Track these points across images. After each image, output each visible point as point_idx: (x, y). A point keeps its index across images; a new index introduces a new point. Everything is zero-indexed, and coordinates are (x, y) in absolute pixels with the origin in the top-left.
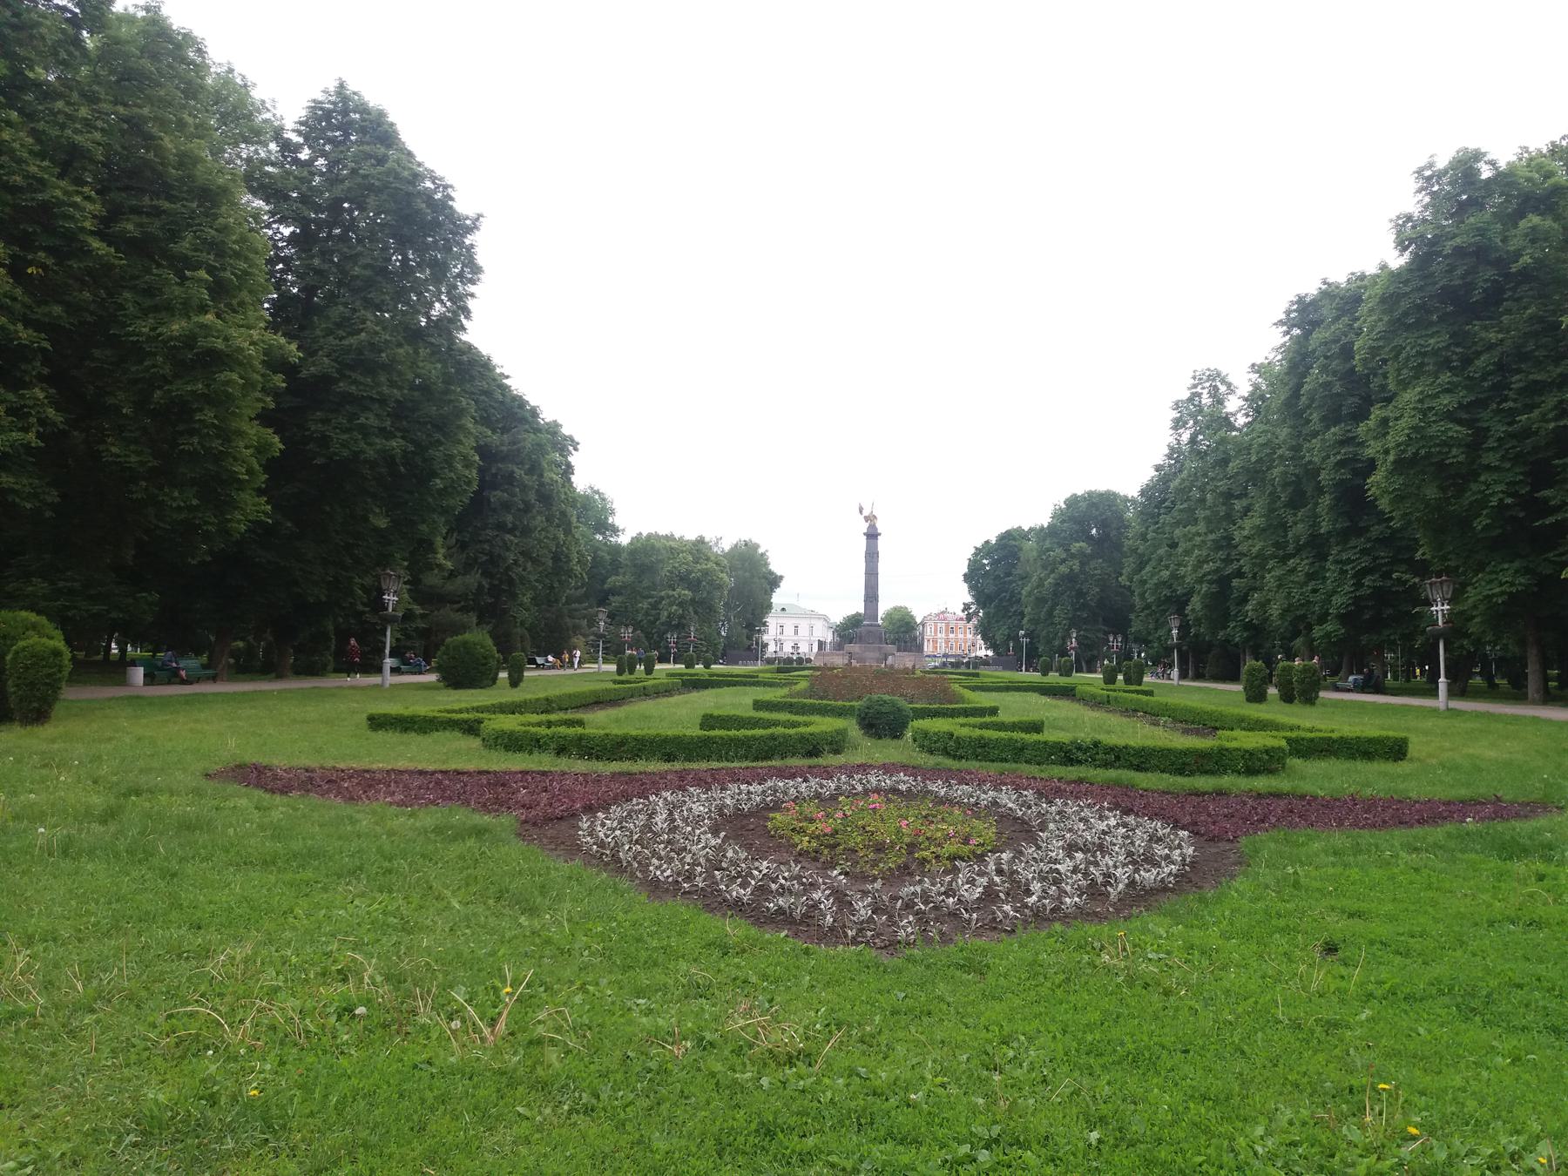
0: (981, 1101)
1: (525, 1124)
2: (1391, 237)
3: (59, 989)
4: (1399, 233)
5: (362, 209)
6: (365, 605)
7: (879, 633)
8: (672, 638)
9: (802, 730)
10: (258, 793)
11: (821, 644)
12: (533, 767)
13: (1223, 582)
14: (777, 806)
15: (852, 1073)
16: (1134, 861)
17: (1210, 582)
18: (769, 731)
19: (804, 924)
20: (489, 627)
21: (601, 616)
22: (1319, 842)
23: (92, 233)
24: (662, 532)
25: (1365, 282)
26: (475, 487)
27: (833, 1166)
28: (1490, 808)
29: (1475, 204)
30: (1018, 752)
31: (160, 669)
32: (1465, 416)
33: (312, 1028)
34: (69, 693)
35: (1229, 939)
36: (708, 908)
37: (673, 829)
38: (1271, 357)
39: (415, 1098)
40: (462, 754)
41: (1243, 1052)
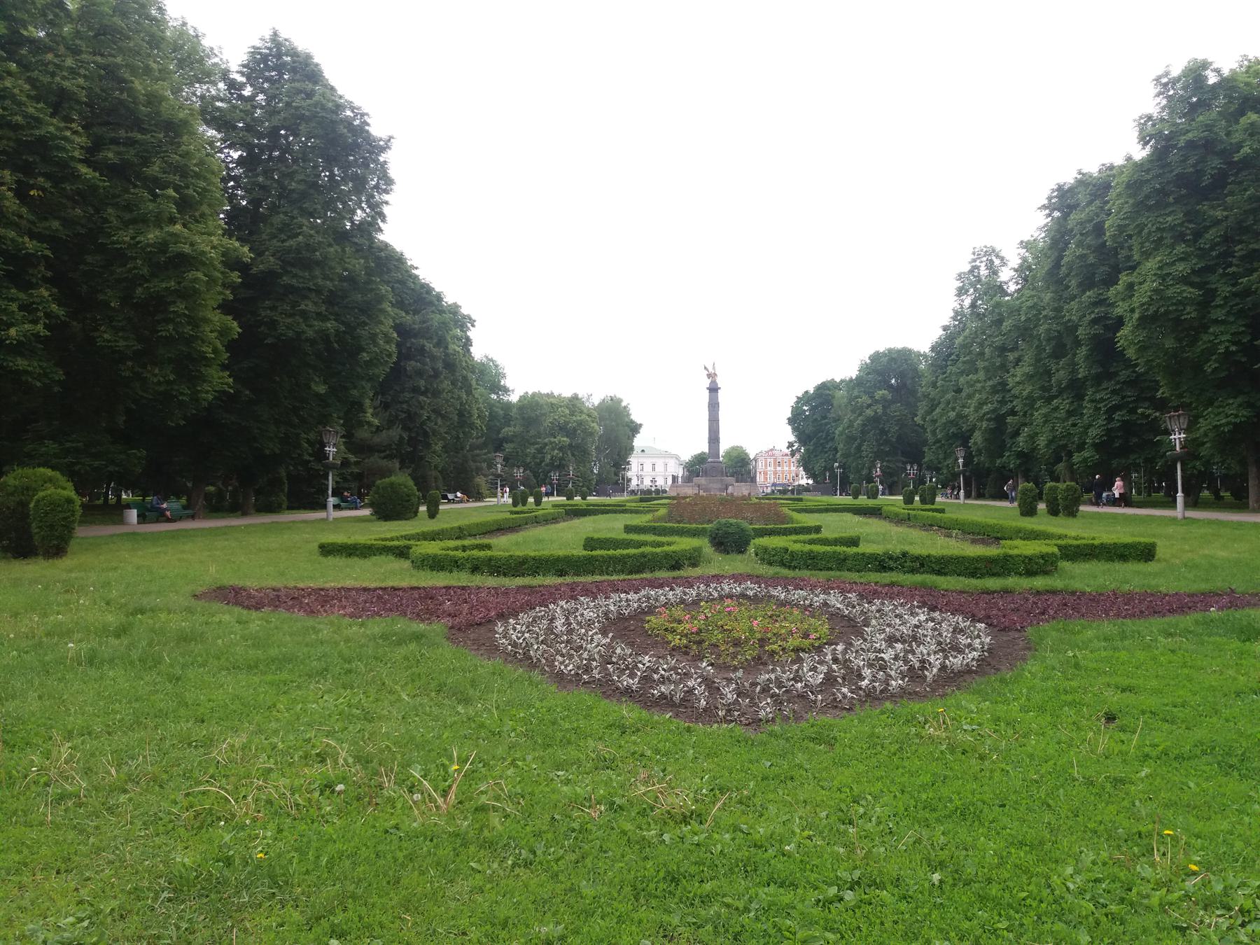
0: (842, 850)
1: (478, 876)
2: (1135, 134)
3: (96, 773)
4: (1141, 131)
5: (296, 135)
6: (310, 455)
8: (555, 476)
9: (666, 548)
10: (237, 610)
11: (674, 478)
12: (454, 583)
13: (1000, 420)
14: (651, 611)
15: (736, 829)
16: (943, 649)
18: (641, 550)
19: (683, 706)
20: (410, 471)
21: (498, 460)
22: (1093, 631)
23: (80, 161)
24: (544, 391)
25: (1114, 171)
26: (395, 359)
27: (728, 906)
28: (1226, 599)
29: (1203, 105)
30: (841, 563)
31: (149, 511)
32: (1197, 280)
33: (301, 802)
34: (81, 532)
35: (1028, 712)
36: (606, 696)
37: (570, 632)
38: (1036, 235)
39: (389, 856)
40: (395, 573)
41: (1049, 806)
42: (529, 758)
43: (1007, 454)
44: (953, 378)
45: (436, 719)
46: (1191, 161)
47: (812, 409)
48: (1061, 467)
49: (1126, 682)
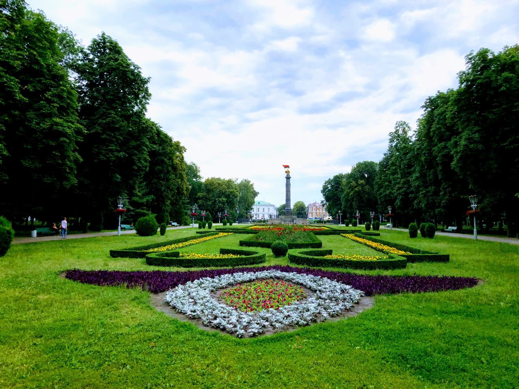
4: (461, 78)
8: (219, 215)
13: (406, 194)
17: (402, 195)
24: (217, 177)
47: (332, 186)
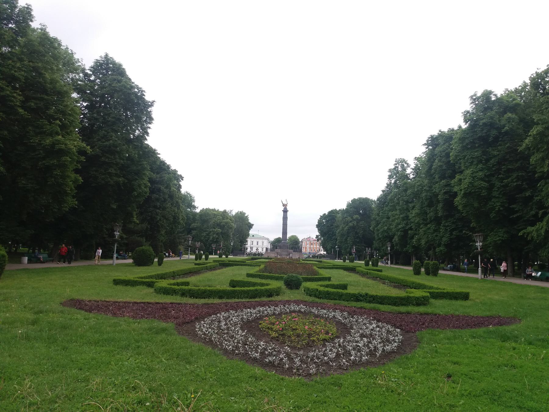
5: (112, 97)
7: (287, 245)
8: (214, 246)
11: (267, 249)
12: (174, 301)
13: (405, 232)
17: (401, 231)
18: (256, 288)
22: (444, 334)
30: (340, 297)
32: (487, 179)
35: (417, 373)
42: (219, 391)
43: (408, 246)
44: (386, 212)
45: (178, 371)
46: (485, 131)
47: (327, 222)
48: (431, 252)
49: (455, 360)
